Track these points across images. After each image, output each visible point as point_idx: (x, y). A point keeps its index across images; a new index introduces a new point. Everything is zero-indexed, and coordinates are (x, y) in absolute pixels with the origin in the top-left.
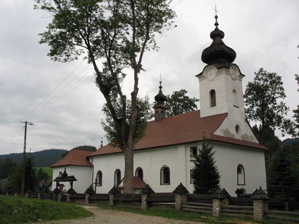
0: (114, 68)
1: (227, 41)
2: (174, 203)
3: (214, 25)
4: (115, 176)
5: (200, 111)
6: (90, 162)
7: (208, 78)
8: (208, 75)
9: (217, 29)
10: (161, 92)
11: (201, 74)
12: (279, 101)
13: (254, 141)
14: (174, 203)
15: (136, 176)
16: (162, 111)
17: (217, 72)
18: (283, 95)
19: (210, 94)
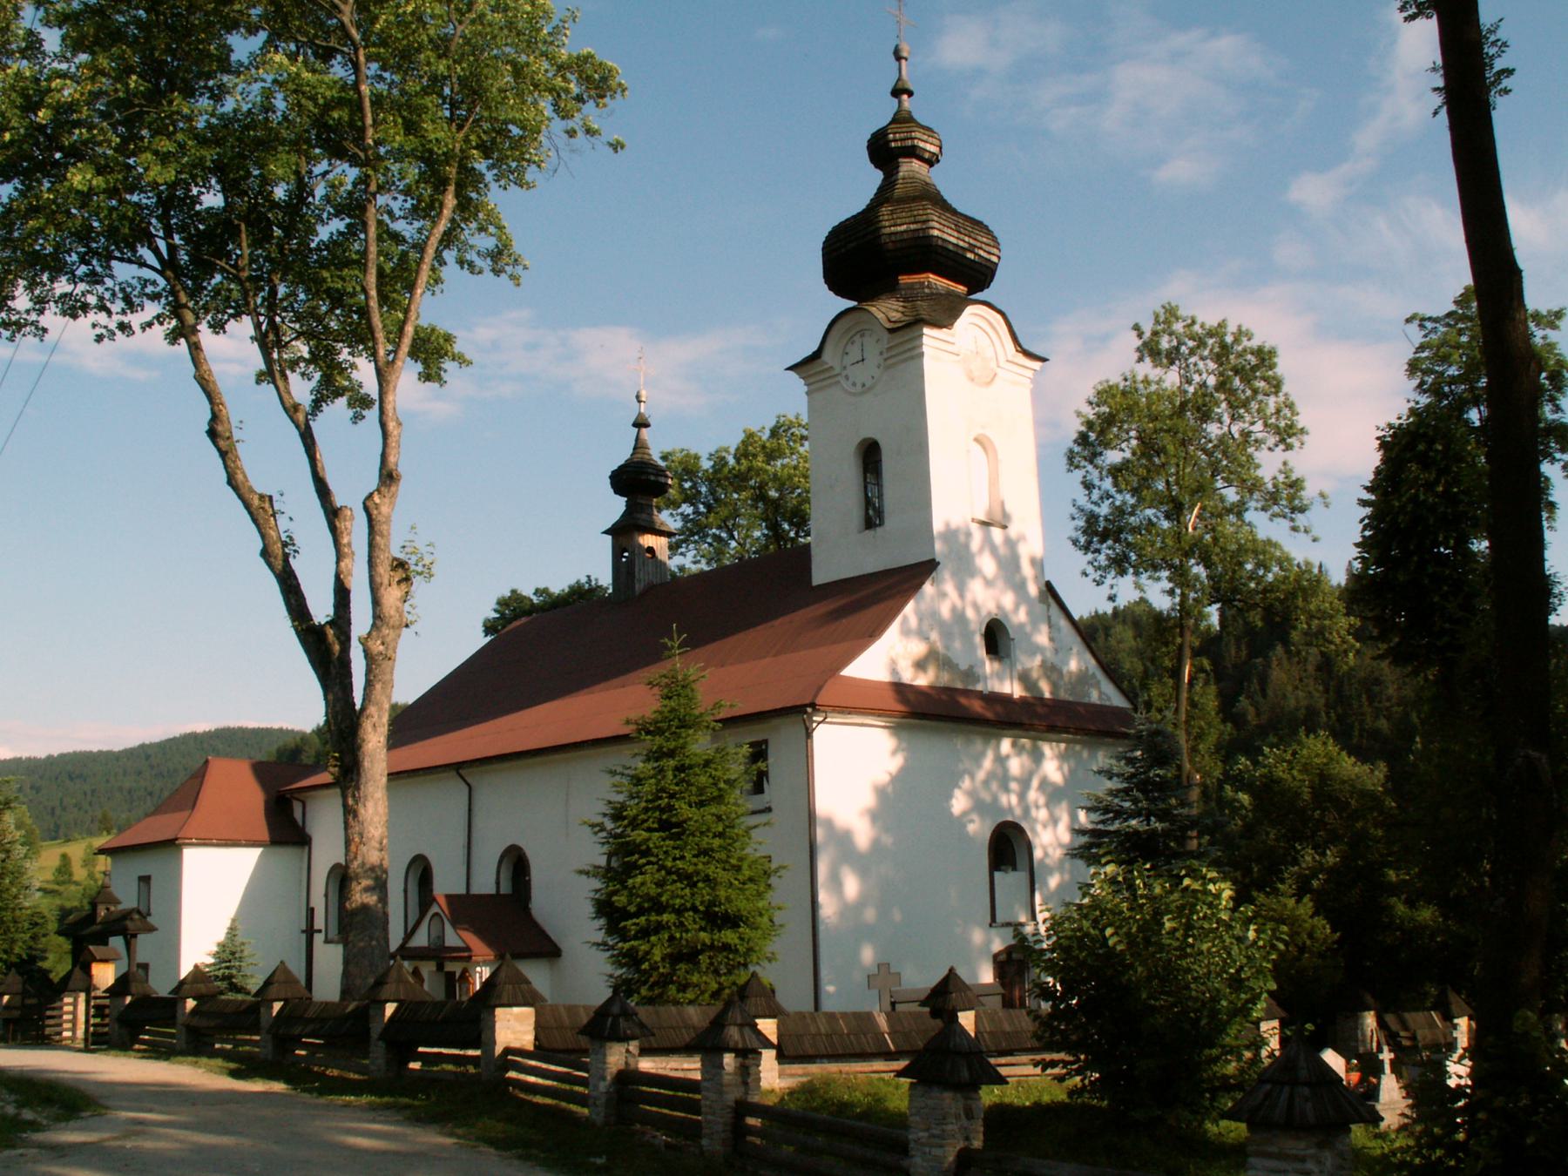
0: (233, 147)
1: (959, 179)
2: (698, 1097)
3: (515, 587)
4: (406, 891)
5: (813, 552)
6: (295, 821)
7: (847, 378)
8: (848, 360)
9: (902, 119)
10: (639, 445)
11: (817, 355)
12: (1268, 464)
13: (1094, 697)
14: (698, 1097)
15: (502, 891)
16: (143, 329)
17: (889, 349)
18: (1287, 434)
19: (860, 462)
